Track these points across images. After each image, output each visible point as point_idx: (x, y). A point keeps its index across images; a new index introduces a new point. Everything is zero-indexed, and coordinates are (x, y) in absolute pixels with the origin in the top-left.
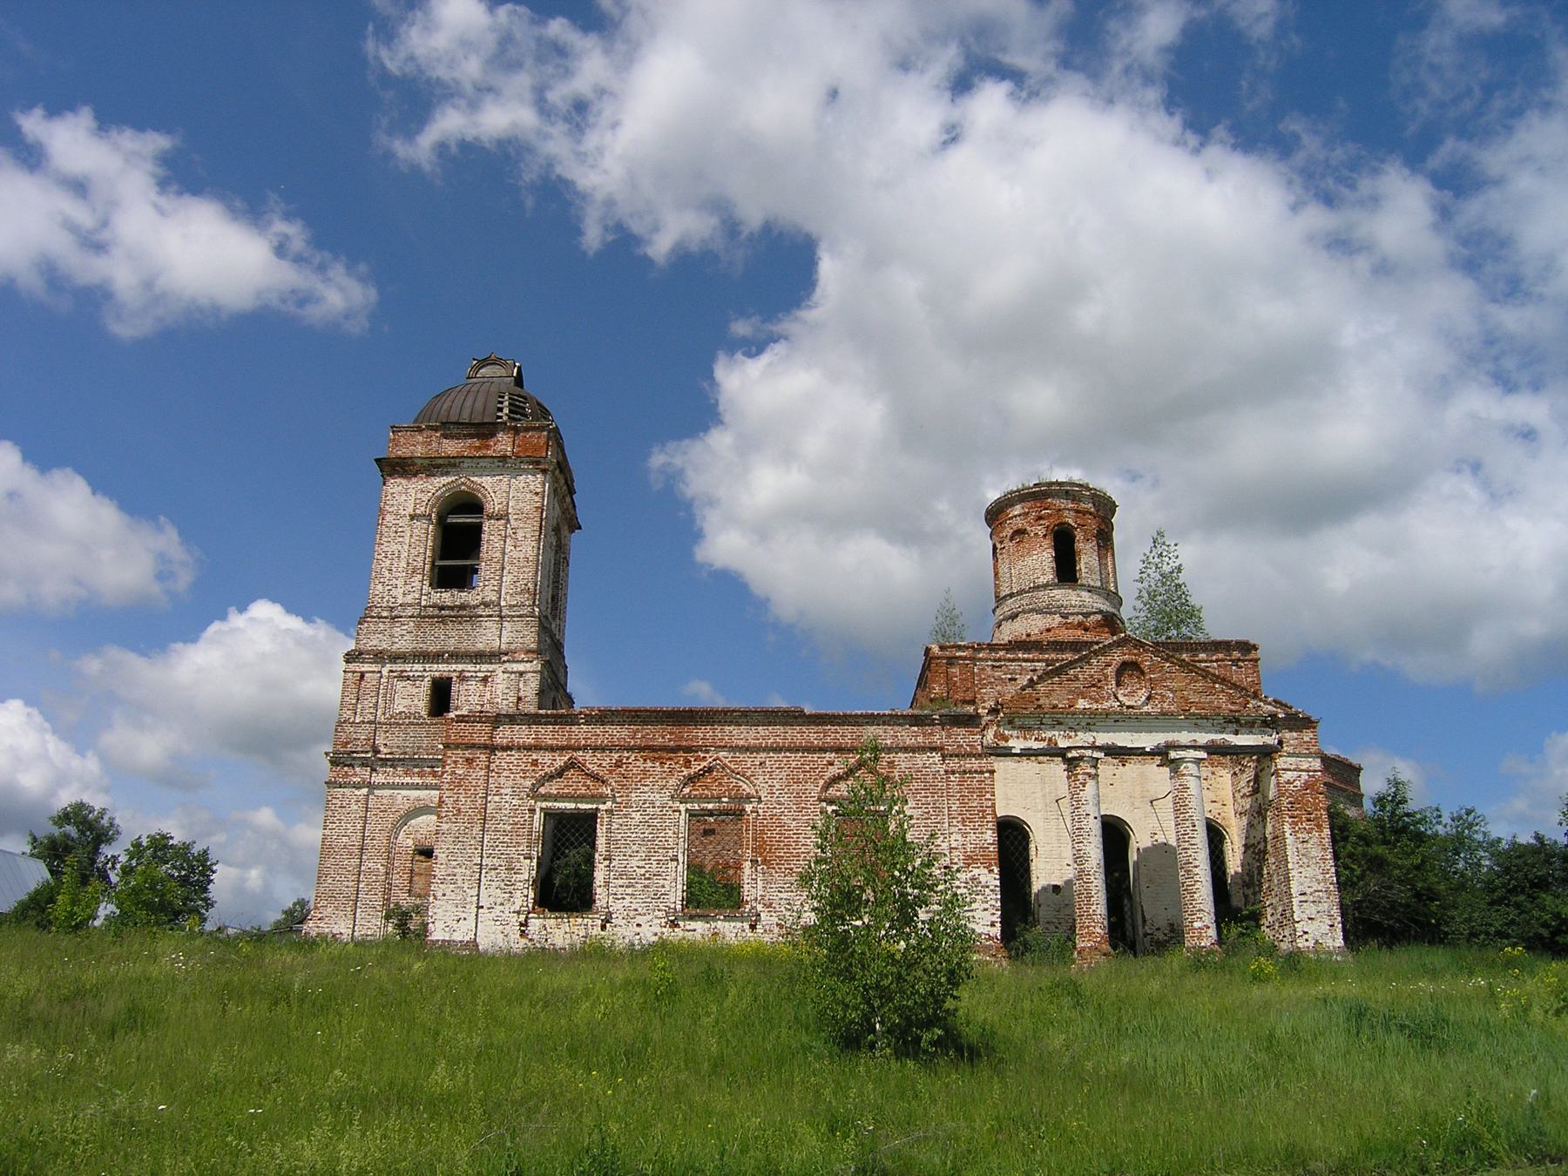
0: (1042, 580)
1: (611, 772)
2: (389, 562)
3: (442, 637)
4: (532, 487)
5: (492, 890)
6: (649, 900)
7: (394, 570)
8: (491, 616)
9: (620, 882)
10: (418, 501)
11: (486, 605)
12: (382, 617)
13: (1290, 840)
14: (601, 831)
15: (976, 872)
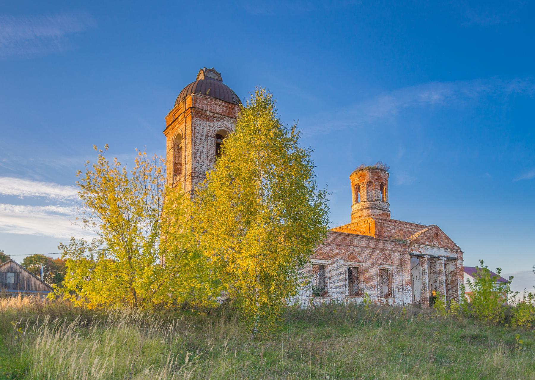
0: (377, 199)
7: (202, 158)
9: (333, 287)
10: (208, 130)
12: (200, 177)
14: (327, 270)
15: (408, 286)
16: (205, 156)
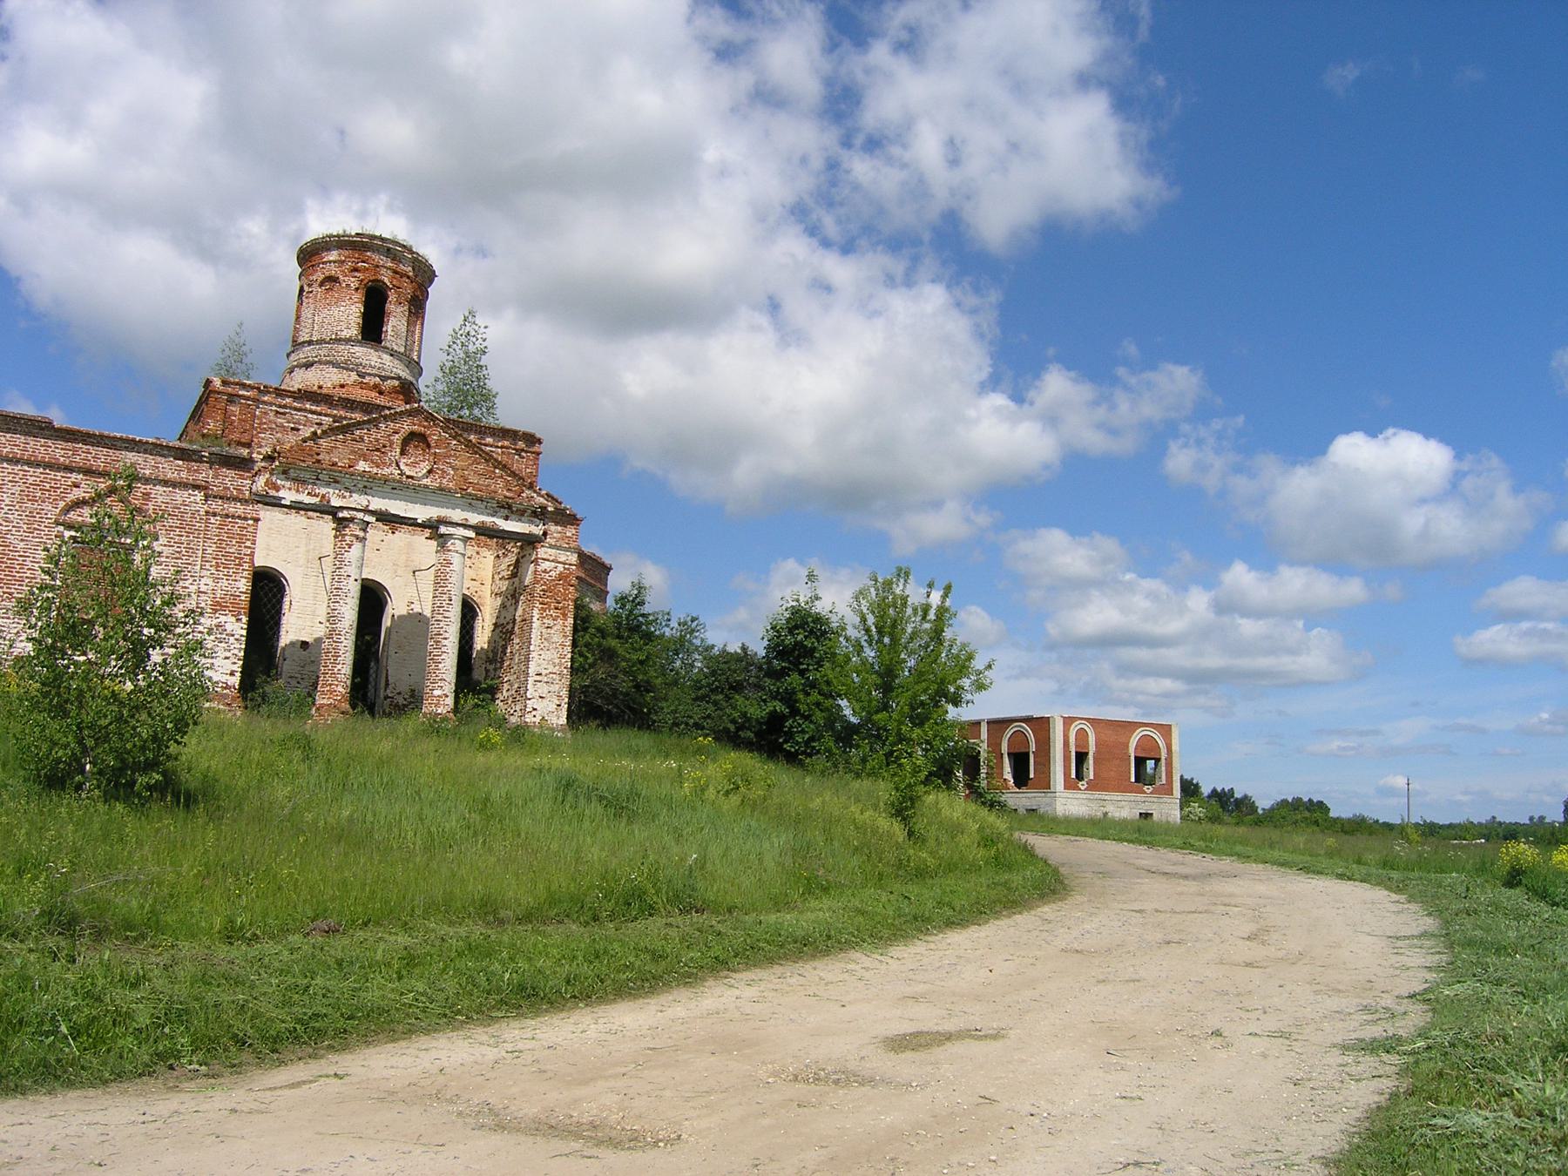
0: (346, 334)
13: (536, 624)
15: (223, 619)
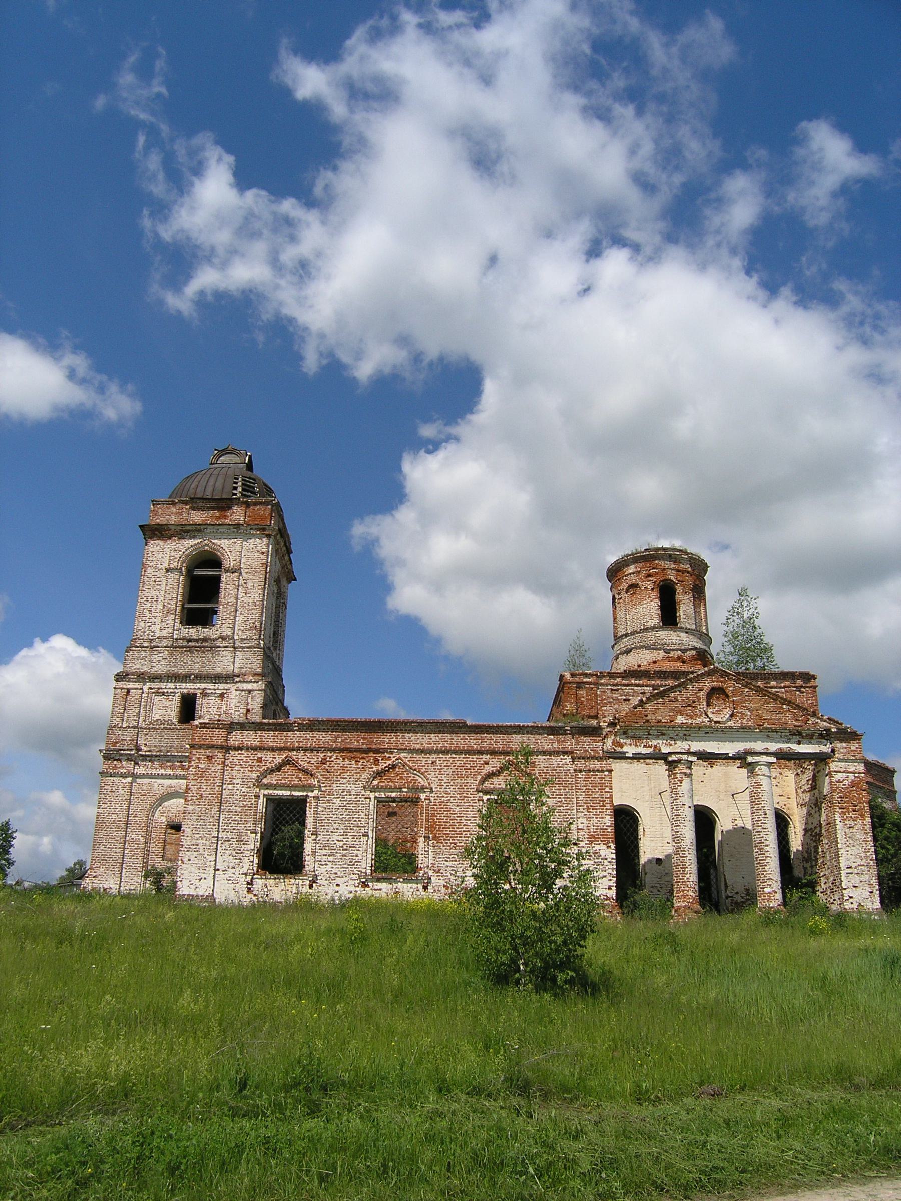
0: (651, 623)
1: (318, 768)
2: (149, 604)
3: (189, 662)
4: (259, 548)
5: (226, 857)
6: (346, 866)
8: (226, 647)
9: (324, 852)
10: (172, 558)
11: (223, 638)
12: (144, 647)
14: (310, 813)
16: (160, 606)
